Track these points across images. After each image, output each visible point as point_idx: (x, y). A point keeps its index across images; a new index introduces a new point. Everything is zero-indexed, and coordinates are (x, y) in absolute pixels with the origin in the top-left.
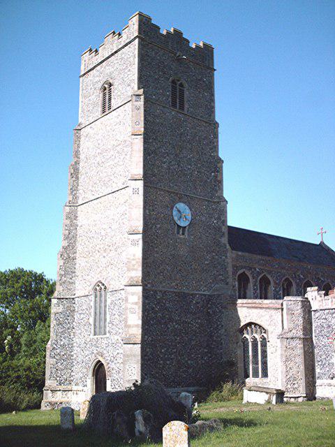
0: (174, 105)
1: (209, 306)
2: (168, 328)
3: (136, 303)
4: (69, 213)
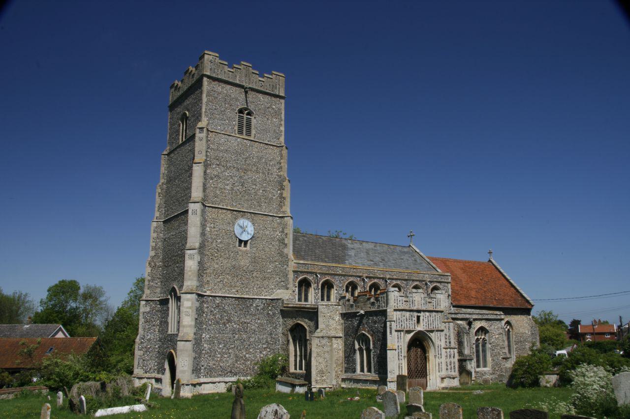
0: (240, 132)
1: (270, 308)
2: (227, 328)
3: (190, 308)
4: (156, 227)
